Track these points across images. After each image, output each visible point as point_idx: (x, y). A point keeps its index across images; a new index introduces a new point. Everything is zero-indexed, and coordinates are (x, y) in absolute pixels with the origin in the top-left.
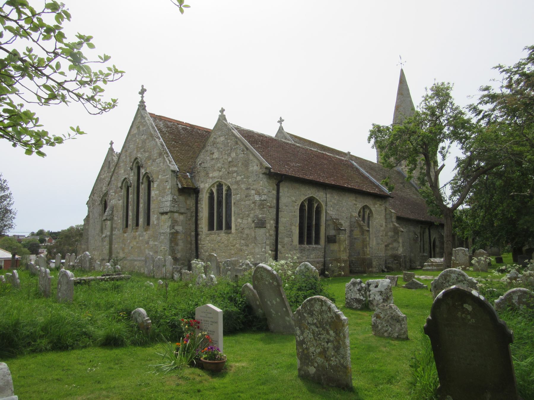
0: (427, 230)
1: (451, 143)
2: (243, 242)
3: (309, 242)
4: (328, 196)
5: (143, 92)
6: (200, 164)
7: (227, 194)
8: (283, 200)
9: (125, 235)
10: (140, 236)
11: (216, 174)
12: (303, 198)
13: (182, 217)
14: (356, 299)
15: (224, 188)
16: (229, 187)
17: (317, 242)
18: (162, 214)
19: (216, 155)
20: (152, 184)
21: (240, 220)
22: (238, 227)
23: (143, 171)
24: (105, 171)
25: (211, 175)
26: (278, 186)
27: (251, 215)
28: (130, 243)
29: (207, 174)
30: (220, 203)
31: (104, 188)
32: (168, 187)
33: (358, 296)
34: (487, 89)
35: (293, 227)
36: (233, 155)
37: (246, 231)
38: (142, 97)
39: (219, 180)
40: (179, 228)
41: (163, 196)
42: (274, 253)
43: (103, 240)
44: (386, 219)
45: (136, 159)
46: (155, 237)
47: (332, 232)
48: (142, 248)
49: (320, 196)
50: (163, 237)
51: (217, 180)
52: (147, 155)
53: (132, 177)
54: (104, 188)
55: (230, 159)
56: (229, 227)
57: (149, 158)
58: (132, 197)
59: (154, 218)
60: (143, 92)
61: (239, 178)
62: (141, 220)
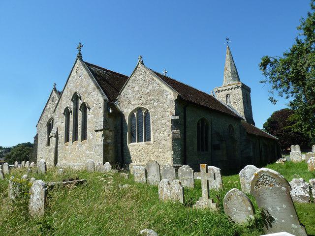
0: (258, 141)
1: (25, 163)
2: (160, 150)
3: (203, 150)
4: (212, 117)
5: (81, 47)
6: (124, 96)
7: (145, 117)
8: (188, 119)
9: (67, 147)
10: (78, 147)
11: (137, 102)
12: (199, 118)
13: (111, 134)
14: (301, 196)
15: (143, 112)
16: (147, 110)
17: (207, 150)
18: (96, 131)
19: (136, 89)
20: (88, 110)
21: (157, 135)
22: (156, 140)
23: (80, 102)
24: (42, 124)
25: (132, 103)
26: (185, 109)
27: (167, 130)
28: (71, 153)
29: (129, 103)
30: (139, 124)
31: (49, 116)
32: (101, 112)
33: (303, 194)
34: (265, 63)
35: (194, 139)
36: (150, 87)
37: (163, 142)
38: (80, 51)
39: (139, 106)
40: (109, 141)
41: (96, 118)
42: (183, 158)
43: (50, 151)
44: (241, 133)
45: (76, 93)
46: (89, 148)
47: (217, 143)
48: (81, 156)
49: (207, 117)
50: (98, 148)
51: (137, 106)
52: (84, 90)
53: (72, 107)
54: (49, 116)
55: (148, 91)
56: (148, 139)
57: (85, 92)
58: (71, 119)
59: (89, 134)
60: (81, 47)
61: (155, 104)
62: (80, 136)
